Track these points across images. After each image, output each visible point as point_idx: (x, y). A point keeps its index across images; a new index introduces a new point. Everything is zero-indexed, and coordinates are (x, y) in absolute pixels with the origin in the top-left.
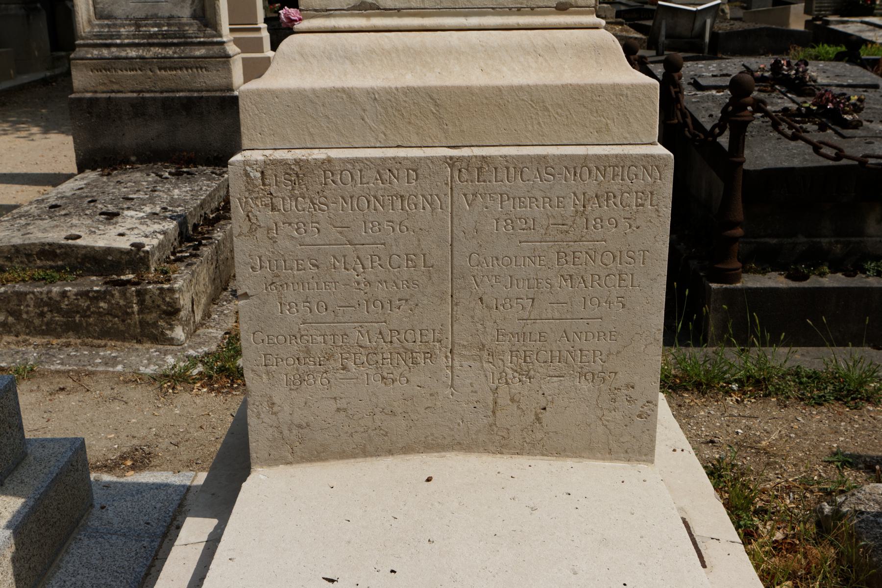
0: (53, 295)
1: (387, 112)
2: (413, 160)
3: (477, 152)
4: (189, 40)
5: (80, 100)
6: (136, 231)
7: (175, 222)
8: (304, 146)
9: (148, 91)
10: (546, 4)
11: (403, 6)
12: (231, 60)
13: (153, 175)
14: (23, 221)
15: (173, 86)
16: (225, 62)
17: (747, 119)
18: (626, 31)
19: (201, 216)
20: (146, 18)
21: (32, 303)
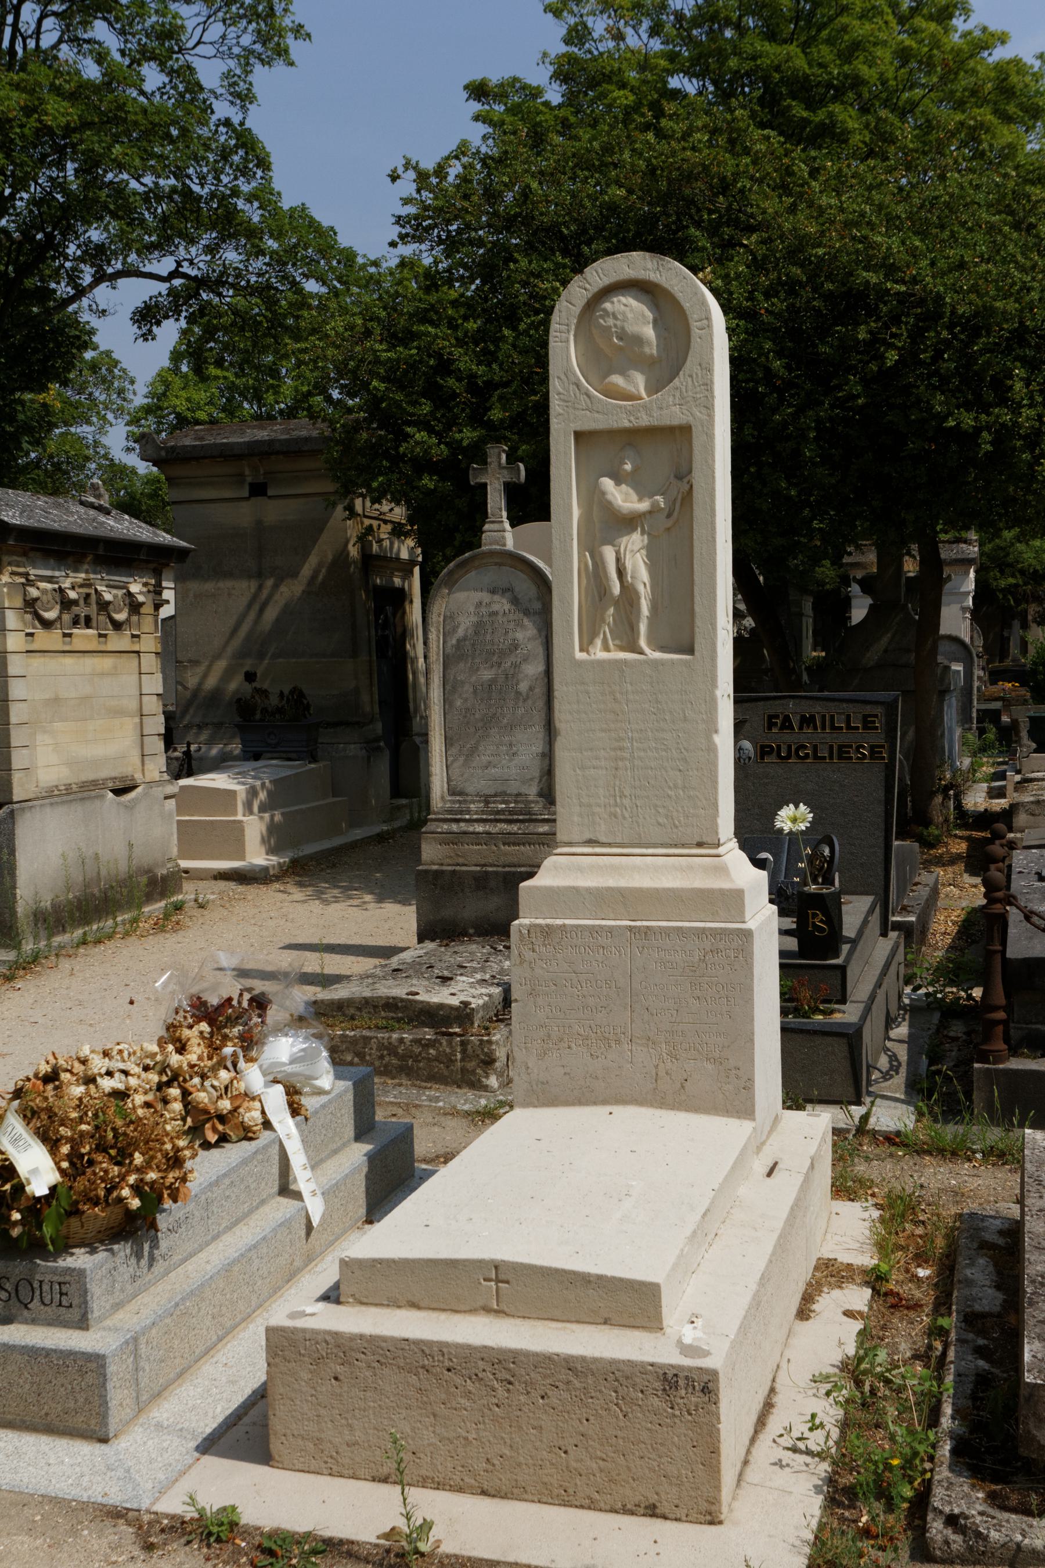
0: (393, 1040)
2: (609, 927)
3: (645, 923)
5: (426, 872)
9: (491, 866)
14: (370, 980)
15: (515, 860)
20: (495, 795)
21: (375, 1047)
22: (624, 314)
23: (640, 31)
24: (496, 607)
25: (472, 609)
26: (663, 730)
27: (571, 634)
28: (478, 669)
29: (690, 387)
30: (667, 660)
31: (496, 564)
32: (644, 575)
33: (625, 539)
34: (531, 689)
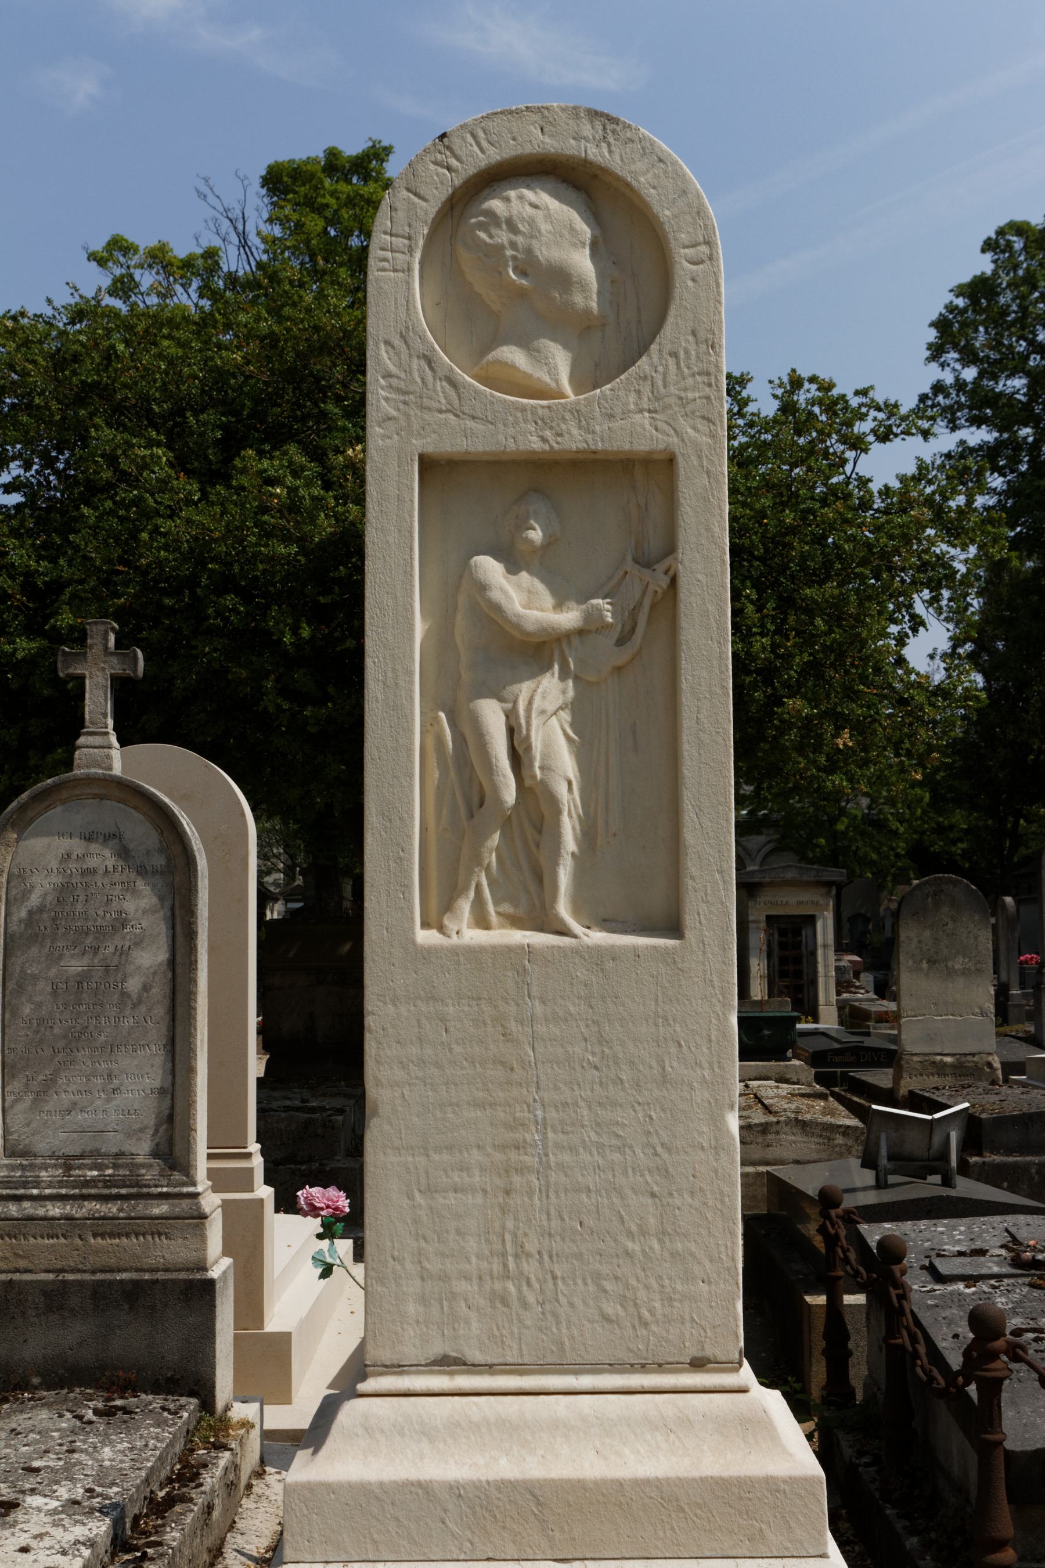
1: (474, 1513)
4: (145, 1190)
6: (47, 1542)
7: (108, 1520)
8: (365, 1558)
9: (72, 1271)
10: (677, 1359)
11: (495, 1361)
12: (207, 1222)
13: (68, 1415)
15: (113, 1262)
16: (197, 1226)
17: (999, 1374)
18: (832, 1114)
19: (145, 1498)
20: (82, 1156)
22: (532, 222)
23: (190, 291)
24: (92, 863)
25: (54, 865)
26: (614, 1104)
27: (407, 887)
28: (61, 957)
29: (672, 376)
30: (624, 948)
31: (95, 797)
32: (567, 764)
33: (525, 689)
34: (146, 988)
